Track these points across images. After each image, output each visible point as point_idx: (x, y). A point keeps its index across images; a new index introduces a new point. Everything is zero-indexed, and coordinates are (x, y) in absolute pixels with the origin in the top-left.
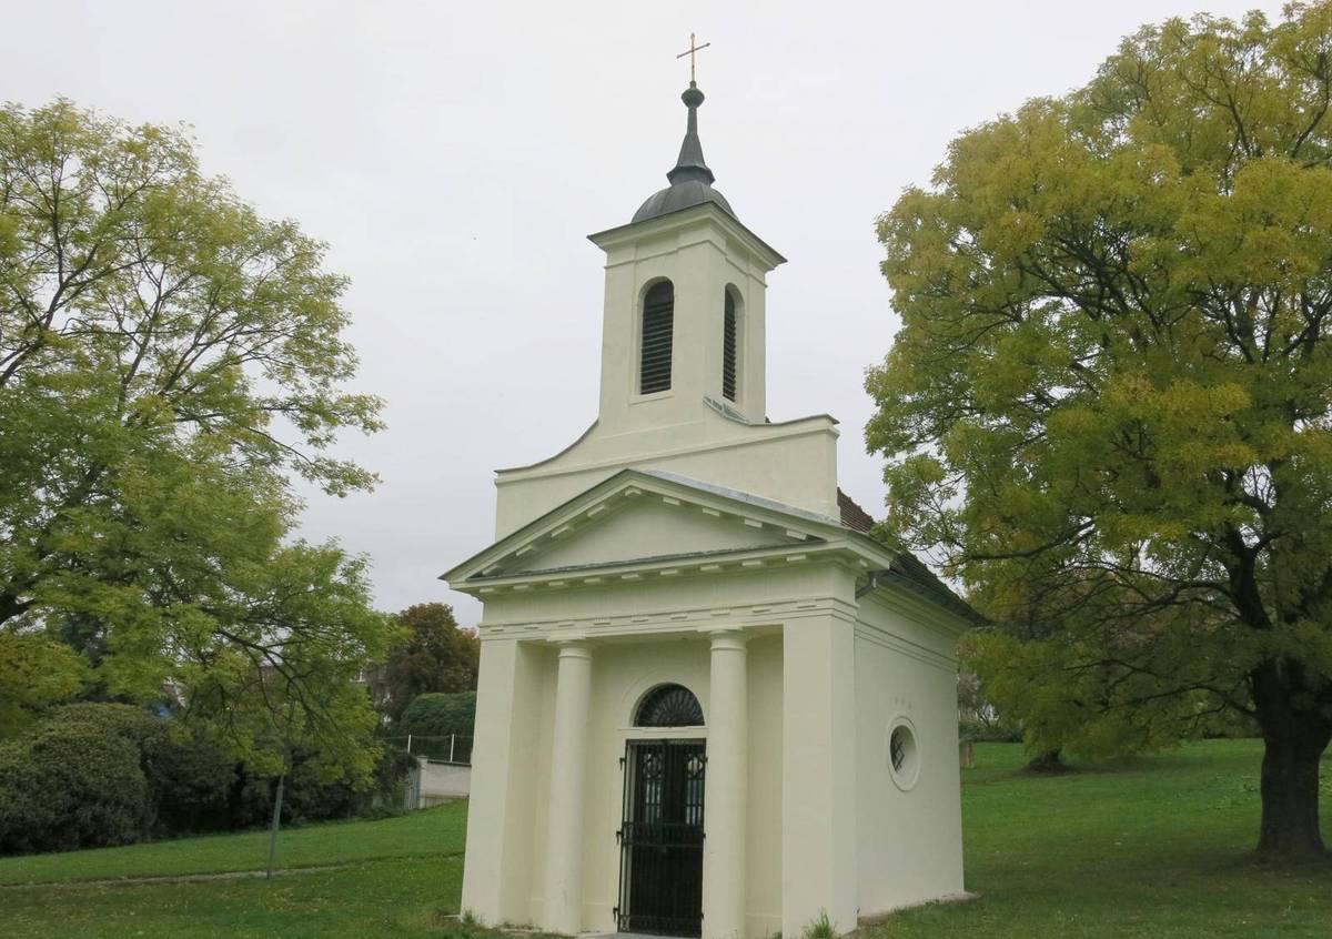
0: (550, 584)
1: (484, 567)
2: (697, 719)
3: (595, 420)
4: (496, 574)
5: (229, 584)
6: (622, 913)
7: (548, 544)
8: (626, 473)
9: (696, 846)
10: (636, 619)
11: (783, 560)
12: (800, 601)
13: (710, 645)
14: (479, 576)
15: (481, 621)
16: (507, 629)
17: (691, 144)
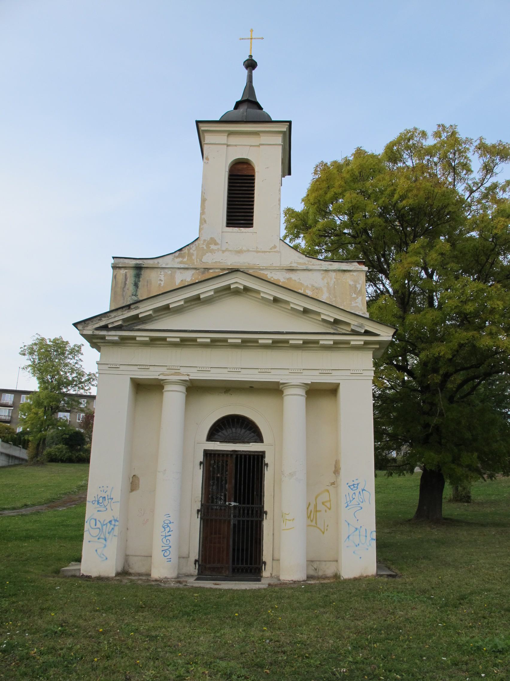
2: (259, 438)
4: (119, 328)
5: (468, 233)
6: (200, 563)
9: (259, 519)
10: (141, 367)
11: (347, 342)
12: (110, 364)
14: (105, 327)
16: (122, 368)
17: (250, 89)
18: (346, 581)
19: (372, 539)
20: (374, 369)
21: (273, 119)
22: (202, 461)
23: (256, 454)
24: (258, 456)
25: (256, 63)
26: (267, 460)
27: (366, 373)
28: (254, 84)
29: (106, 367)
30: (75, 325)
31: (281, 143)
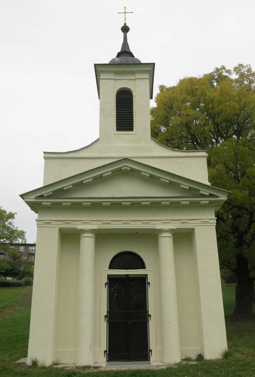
0: (83, 203)
1: (45, 193)
2: (143, 266)
3: (98, 138)
4: (49, 197)
6: (108, 353)
7: (81, 186)
8: (126, 159)
10: (124, 222)
13: (158, 236)
14: (42, 196)
15: (37, 218)
16: (53, 223)
17: (125, 44)
18: (206, 360)
19: (135, 96)
20: (216, 218)
21: (142, 62)
22: (107, 282)
23: (142, 276)
24: (143, 278)
25: (129, 28)
26: (149, 280)
27: (210, 221)
28: (128, 42)
29: (42, 223)
30: (22, 196)
31: (148, 77)
